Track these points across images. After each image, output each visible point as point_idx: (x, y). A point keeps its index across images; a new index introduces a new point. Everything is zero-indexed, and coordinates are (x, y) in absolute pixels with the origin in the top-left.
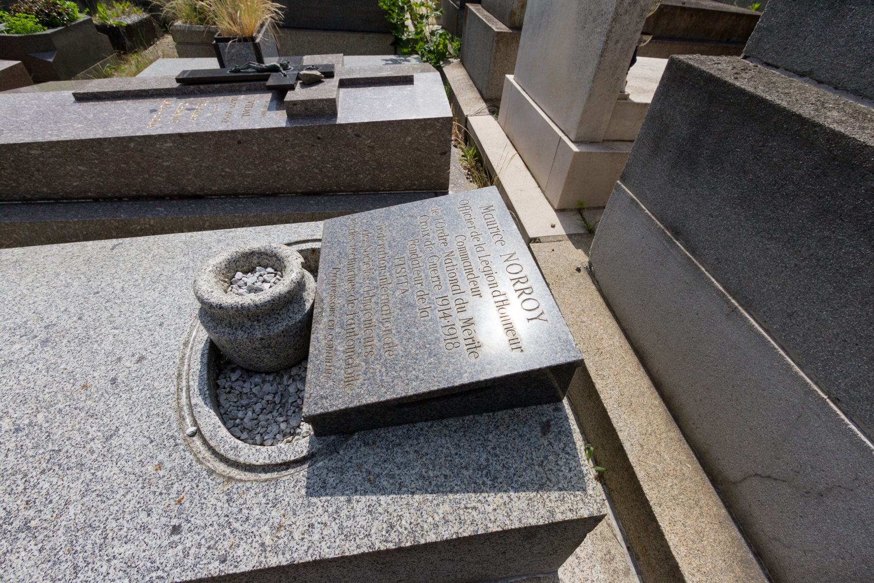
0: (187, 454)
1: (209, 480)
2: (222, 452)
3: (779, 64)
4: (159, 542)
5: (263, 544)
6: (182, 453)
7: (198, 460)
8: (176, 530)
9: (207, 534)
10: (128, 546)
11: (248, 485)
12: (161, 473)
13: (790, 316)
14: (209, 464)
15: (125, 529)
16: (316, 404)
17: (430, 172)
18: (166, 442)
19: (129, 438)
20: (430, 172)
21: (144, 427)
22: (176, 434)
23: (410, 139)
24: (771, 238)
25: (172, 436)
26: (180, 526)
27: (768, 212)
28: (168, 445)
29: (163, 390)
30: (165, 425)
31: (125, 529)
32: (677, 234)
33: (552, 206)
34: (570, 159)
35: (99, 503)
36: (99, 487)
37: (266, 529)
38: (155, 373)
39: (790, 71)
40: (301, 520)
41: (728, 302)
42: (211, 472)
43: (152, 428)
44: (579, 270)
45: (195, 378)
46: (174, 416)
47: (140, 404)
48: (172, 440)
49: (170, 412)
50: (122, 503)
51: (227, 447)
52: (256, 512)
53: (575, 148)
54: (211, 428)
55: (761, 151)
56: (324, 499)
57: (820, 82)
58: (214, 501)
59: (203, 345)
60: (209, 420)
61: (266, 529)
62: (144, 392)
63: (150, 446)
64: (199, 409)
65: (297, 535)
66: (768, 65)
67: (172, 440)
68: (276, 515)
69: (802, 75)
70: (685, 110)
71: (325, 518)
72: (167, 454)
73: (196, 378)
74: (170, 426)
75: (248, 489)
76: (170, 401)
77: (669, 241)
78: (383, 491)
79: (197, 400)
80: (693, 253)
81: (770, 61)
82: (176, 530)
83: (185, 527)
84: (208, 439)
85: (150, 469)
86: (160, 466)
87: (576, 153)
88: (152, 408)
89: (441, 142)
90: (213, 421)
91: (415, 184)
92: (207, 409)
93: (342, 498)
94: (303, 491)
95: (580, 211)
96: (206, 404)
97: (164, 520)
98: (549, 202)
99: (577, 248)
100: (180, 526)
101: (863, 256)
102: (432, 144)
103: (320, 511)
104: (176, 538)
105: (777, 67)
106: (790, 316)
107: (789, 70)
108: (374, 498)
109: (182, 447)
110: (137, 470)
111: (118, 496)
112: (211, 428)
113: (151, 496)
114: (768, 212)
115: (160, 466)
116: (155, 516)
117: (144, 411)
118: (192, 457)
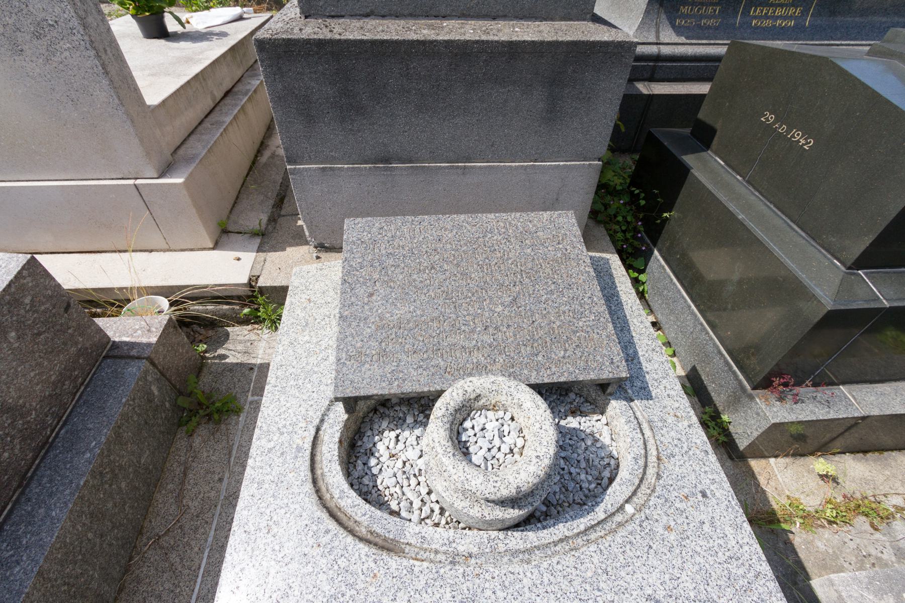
0: (651, 503)
1: (665, 476)
2: (641, 470)
3: (343, 14)
4: (716, 507)
5: (689, 426)
6: (652, 509)
7: (653, 491)
8: (704, 495)
9: (697, 469)
10: (727, 533)
11: (658, 443)
12: (672, 524)
13: (492, 146)
14: (653, 481)
15: (719, 541)
16: (618, 367)
17: (76, 343)
18: (647, 531)
19: (653, 578)
20: (76, 343)
21: (639, 564)
22: (637, 522)
23: (13, 334)
24: (455, 117)
25: (641, 526)
26: (701, 492)
27: (441, 105)
28: (649, 528)
29: (595, 561)
30: (632, 538)
31: (719, 541)
32: (387, 160)
33: (210, 249)
34: (185, 192)
35: (712, 579)
36: (702, 588)
37: (680, 425)
38: (575, 583)
39: (356, 15)
40: (667, 402)
41: (458, 167)
42: (659, 477)
43: (638, 553)
44: (318, 258)
45: (575, 526)
46: (622, 532)
47: (616, 583)
48: (644, 525)
49: (619, 540)
50: (705, 554)
51: (636, 467)
52: (673, 434)
53: (177, 180)
54: (624, 487)
55: (408, 73)
56: (651, 389)
57: (383, 17)
58: (677, 469)
59: (530, 534)
60: (616, 493)
61: (680, 425)
62: (602, 585)
63: (654, 547)
64: (609, 506)
65: (677, 405)
66: (333, 17)
67: (644, 525)
68: (670, 419)
69: (367, 15)
70: (314, 76)
71: (662, 387)
72: (656, 524)
73: (575, 523)
74: (631, 533)
75: (662, 442)
76: (607, 545)
77: (386, 169)
78: (636, 352)
79: (600, 513)
80: (411, 162)
81: (333, 14)
82: (704, 495)
83: (700, 488)
84: (634, 487)
85: (672, 537)
86: (668, 528)
87: (184, 182)
88: (618, 565)
89: (51, 297)
90: (618, 487)
91: (77, 377)
92: (607, 497)
93: (647, 377)
94: (651, 402)
95: (225, 232)
96: (602, 501)
97: (702, 508)
98: (192, 250)
99: (284, 249)
100: (701, 492)
101: (503, 93)
102: (45, 312)
103: (658, 390)
104: (708, 492)
105: (342, 16)
106: (492, 146)
107: (353, 16)
108: (641, 358)
109: (647, 511)
110: (678, 551)
111: (702, 561)
112: (624, 487)
113: (692, 525)
114: (441, 105)
115: (668, 528)
116: (703, 517)
117: (623, 574)
118: (652, 498)
